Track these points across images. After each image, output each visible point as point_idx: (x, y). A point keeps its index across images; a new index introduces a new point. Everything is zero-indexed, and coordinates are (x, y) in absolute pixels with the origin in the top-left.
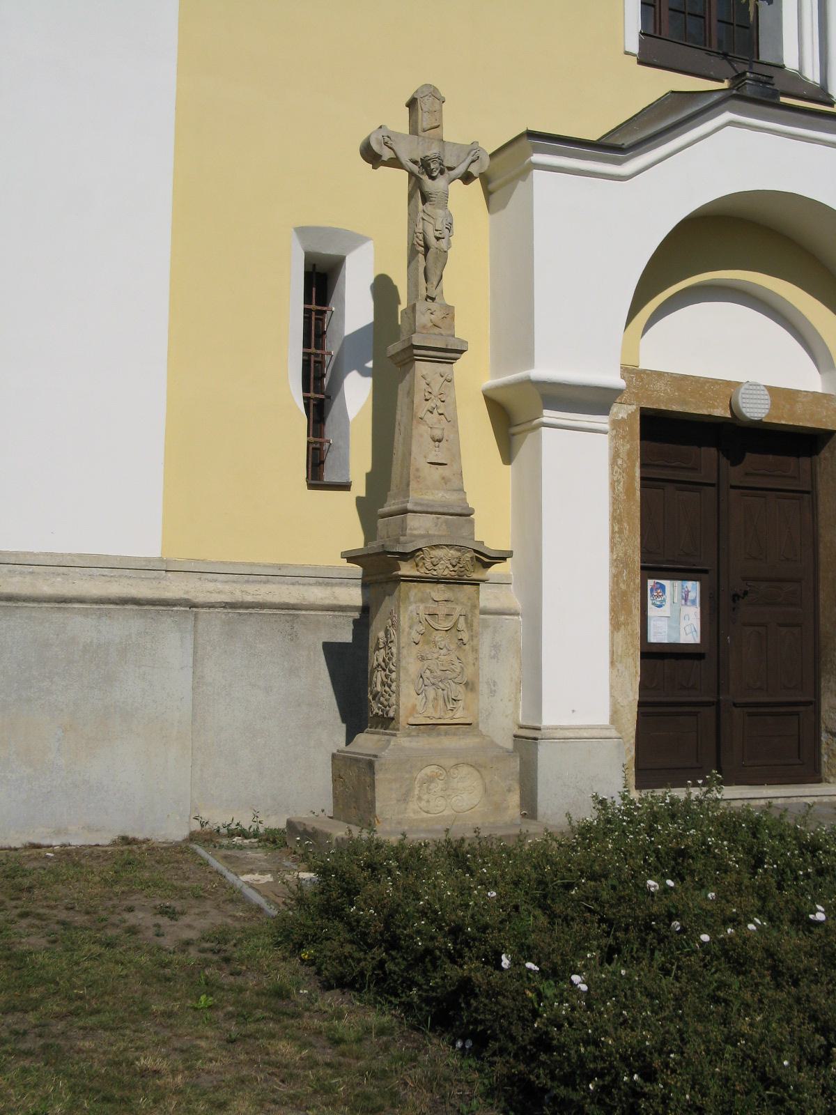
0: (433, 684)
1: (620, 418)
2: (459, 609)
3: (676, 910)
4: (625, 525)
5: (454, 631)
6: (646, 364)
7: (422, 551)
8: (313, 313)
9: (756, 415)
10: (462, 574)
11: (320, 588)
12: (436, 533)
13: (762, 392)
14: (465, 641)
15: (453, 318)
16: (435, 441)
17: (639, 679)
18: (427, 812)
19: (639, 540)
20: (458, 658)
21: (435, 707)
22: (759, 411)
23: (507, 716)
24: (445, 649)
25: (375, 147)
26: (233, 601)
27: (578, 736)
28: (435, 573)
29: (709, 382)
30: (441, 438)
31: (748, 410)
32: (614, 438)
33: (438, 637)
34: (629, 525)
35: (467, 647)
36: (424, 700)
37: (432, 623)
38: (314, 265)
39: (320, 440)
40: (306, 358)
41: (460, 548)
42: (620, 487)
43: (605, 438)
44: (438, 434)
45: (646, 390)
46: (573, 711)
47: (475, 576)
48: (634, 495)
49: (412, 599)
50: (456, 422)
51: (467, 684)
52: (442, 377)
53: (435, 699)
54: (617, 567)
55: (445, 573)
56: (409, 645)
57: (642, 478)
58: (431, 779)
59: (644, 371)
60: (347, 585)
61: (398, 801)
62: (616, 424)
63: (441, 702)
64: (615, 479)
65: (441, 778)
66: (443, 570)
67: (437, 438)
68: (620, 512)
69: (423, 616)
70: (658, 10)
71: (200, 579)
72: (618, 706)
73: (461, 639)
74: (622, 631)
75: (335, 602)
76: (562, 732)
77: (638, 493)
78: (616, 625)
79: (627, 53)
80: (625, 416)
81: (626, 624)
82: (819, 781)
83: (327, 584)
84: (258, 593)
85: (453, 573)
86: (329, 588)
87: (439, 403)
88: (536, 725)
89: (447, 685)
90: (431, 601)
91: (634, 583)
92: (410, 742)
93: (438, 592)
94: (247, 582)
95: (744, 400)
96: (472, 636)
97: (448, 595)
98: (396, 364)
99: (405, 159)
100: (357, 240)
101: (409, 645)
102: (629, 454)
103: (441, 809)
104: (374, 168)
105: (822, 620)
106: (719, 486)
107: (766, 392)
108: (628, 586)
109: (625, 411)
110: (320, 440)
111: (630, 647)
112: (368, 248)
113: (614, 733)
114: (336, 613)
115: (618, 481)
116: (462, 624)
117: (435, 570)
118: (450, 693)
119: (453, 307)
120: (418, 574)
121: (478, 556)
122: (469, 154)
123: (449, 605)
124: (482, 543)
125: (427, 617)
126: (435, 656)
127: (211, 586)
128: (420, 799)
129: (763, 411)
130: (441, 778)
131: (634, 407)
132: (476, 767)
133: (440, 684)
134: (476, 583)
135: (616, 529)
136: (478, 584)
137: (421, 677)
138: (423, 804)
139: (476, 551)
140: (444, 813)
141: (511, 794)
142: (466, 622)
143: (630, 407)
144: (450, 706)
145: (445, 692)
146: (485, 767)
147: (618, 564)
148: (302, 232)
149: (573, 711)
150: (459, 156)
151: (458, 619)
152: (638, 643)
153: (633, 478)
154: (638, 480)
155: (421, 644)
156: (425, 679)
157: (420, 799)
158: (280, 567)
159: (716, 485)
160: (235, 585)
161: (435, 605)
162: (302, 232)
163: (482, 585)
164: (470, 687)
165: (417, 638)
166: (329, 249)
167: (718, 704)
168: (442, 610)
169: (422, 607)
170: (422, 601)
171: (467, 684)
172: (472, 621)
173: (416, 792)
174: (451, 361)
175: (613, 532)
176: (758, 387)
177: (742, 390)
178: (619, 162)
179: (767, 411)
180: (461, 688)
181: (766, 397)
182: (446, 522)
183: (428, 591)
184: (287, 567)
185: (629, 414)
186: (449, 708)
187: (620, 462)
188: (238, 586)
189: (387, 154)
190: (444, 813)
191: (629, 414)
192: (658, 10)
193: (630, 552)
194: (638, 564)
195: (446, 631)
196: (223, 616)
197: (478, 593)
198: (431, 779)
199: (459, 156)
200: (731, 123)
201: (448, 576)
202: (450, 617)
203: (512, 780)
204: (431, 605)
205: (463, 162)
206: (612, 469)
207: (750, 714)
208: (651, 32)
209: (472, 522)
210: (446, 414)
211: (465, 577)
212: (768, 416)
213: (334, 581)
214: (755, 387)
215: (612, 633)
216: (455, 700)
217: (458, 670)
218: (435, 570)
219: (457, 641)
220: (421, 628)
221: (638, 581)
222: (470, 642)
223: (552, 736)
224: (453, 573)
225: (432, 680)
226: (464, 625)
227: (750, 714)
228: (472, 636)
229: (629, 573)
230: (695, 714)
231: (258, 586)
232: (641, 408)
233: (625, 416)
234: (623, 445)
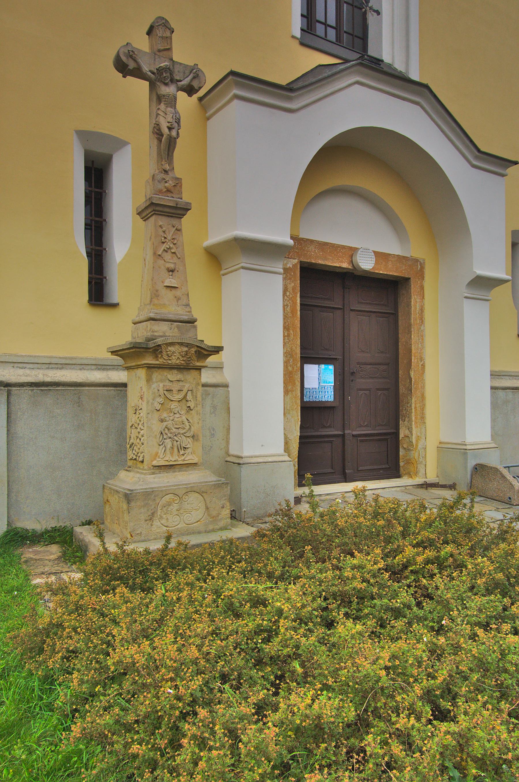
0: (170, 438)
1: (288, 267)
2: (187, 386)
3: (396, 703)
4: (291, 331)
5: (184, 401)
6: (303, 235)
7: (161, 346)
8: (93, 193)
9: (367, 267)
10: (189, 362)
11: (99, 371)
12: (171, 335)
13: (370, 254)
14: (192, 408)
15: (181, 186)
16: (169, 272)
17: (300, 423)
18: (167, 527)
19: (299, 341)
20: (187, 420)
21: (172, 454)
22: (369, 265)
23: (221, 449)
24: (178, 414)
25: (124, 59)
26: (37, 381)
27: (265, 461)
28: (170, 362)
29: (339, 247)
30: (173, 268)
31: (362, 264)
32: (284, 279)
33: (173, 405)
34: (293, 331)
35: (193, 412)
36: (164, 449)
37: (169, 396)
38: (93, 161)
39: (101, 277)
40: (89, 222)
41: (188, 345)
42: (288, 309)
43: (281, 277)
44: (172, 266)
45: (304, 250)
46: (262, 446)
47: (198, 364)
48: (297, 313)
49: (154, 380)
50: (184, 259)
51: (193, 437)
52: (174, 227)
53: (172, 448)
54: (286, 357)
55: (178, 362)
56: (153, 412)
57: (301, 304)
58: (169, 504)
59: (302, 239)
60: (117, 369)
61: (146, 521)
62: (286, 270)
63: (176, 450)
64: (285, 304)
65: (176, 502)
66: (174, 361)
67: (170, 269)
68: (288, 324)
69: (161, 392)
70: (310, 20)
71: (13, 367)
72: (288, 440)
73: (189, 407)
74: (290, 395)
75: (109, 381)
76: (255, 459)
77: (299, 313)
78: (286, 392)
79: (293, 37)
80: (291, 266)
81: (292, 391)
82: (398, 476)
83: (104, 369)
84: (55, 376)
85: (183, 362)
86: (105, 372)
87: (172, 246)
88: (240, 454)
89: (180, 438)
90: (168, 381)
91: (297, 367)
92: (154, 478)
93: (174, 375)
94: (48, 368)
95: (360, 258)
96: (197, 404)
97: (180, 376)
98: (142, 218)
99: (146, 68)
100: (121, 144)
101: (153, 412)
102: (294, 289)
103: (176, 523)
104: (124, 77)
105: (401, 387)
106: (344, 310)
107: (373, 254)
108: (293, 368)
109: (293, 262)
110: (101, 277)
111: (295, 404)
112: (128, 149)
113: (287, 458)
114: (110, 388)
115: (287, 305)
116: (189, 397)
117: (170, 360)
118: (181, 444)
119: (181, 179)
120: (158, 362)
121: (199, 349)
122: (191, 72)
123: (181, 383)
124: (203, 341)
125: (166, 392)
126: (171, 418)
127: (21, 372)
128: (161, 517)
129: (371, 265)
130: (176, 502)
131: (297, 260)
132: (201, 493)
133: (175, 437)
134: (199, 369)
135: (286, 334)
136: (200, 369)
137: (161, 433)
138: (163, 521)
139: (197, 346)
140: (179, 526)
141: (224, 509)
142: (192, 395)
143: (294, 261)
144: (182, 452)
145: (178, 443)
146: (206, 493)
147: (288, 355)
148: (82, 135)
149: (262, 446)
150: (184, 73)
151: (187, 393)
152: (299, 402)
153: (295, 303)
154: (299, 305)
155: (161, 411)
156: (164, 434)
157: (161, 517)
158: (71, 358)
159: (342, 309)
160: (39, 371)
161: (170, 384)
162: (82, 135)
163: (203, 371)
164: (196, 438)
165: (158, 407)
166: (101, 149)
167: (343, 436)
168: (175, 387)
169: (161, 385)
170: (161, 381)
171: (193, 437)
172: (196, 393)
173: (159, 513)
174: (180, 216)
175: (284, 336)
176: (368, 251)
177: (359, 252)
178: (290, 99)
179: (373, 265)
180: (190, 440)
181: (373, 257)
182: (178, 327)
183: (166, 374)
184: (76, 358)
185: (293, 265)
186: (181, 453)
187: (288, 294)
188: (41, 371)
189: (132, 65)
190: (179, 526)
191: (293, 265)
192: (310, 20)
193: (294, 348)
194: (299, 355)
195: (179, 401)
196: (30, 392)
197: (200, 375)
198: (169, 504)
199: (184, 73)
200: (358, 83)
201: (180, 364)
202: (182, 392)
203: (225, 500)
204: (167, 383)
205: (187, 77)
206: (284, 297)
207: (362, 441)
208: (305, 28)
209: (195, 327)
210: (177, 253)
211: (191, 364)
212: (373, 268)
213: (108, 367)
214: (366, 251)
215: (284, 396)
216: (185, 448)
217: (188, 427)
218: (170, 360)
219: (186, 408)
220: (161, 400)
221: (299, 365)
222: (196, 408)
223: (249, 461)
224: (183, 362)
225: (169, 435)
226: (191, 397)
227: (362, 441)
228: (197, 404)
229: (294, 361)
230: (331, 442)
231: (55, 371)
232: (301, 262)
233: (291, 266)
234: (290, 284)
